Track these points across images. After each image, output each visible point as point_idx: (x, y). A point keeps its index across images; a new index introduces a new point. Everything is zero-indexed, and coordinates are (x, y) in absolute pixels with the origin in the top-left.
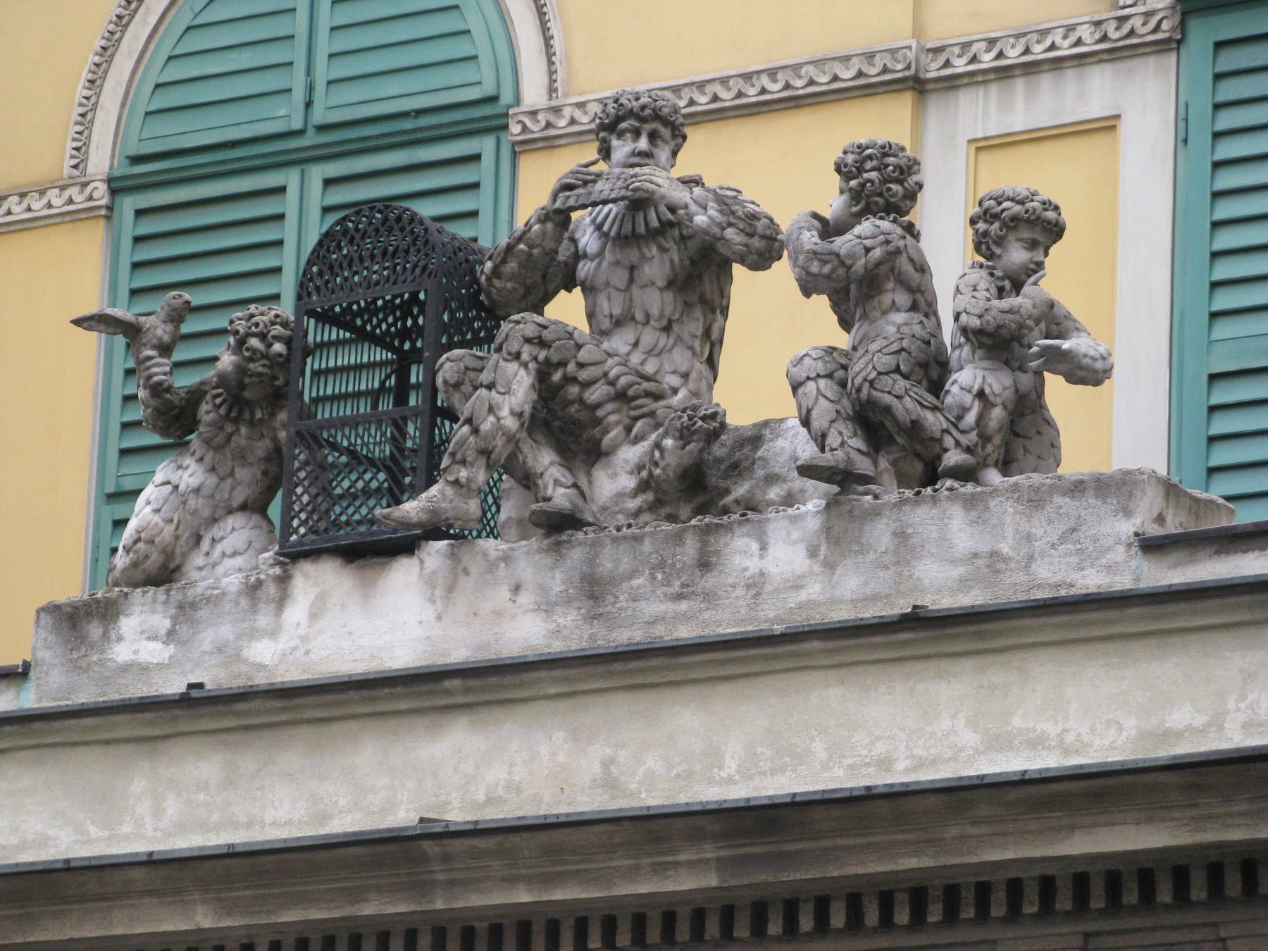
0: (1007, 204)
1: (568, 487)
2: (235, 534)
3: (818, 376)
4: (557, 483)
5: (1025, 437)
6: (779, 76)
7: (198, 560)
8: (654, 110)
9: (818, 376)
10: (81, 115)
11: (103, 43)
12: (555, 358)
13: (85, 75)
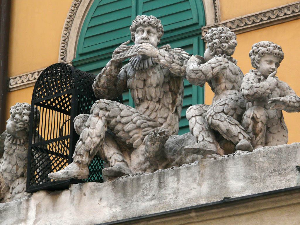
0: (260, 48)
1: (120, 162)
2: (19, 186)
3: (196, 115)
4: (116, 160)
5: (274, 133)
6: (290, 9)
7: (8, 196)
8: (148, 23)
9: (196, 115)
10: (63, 40)
11: (70, 14)
12: (111, 115)
13: (64, 26)
